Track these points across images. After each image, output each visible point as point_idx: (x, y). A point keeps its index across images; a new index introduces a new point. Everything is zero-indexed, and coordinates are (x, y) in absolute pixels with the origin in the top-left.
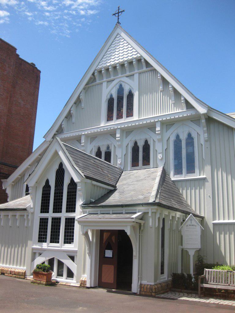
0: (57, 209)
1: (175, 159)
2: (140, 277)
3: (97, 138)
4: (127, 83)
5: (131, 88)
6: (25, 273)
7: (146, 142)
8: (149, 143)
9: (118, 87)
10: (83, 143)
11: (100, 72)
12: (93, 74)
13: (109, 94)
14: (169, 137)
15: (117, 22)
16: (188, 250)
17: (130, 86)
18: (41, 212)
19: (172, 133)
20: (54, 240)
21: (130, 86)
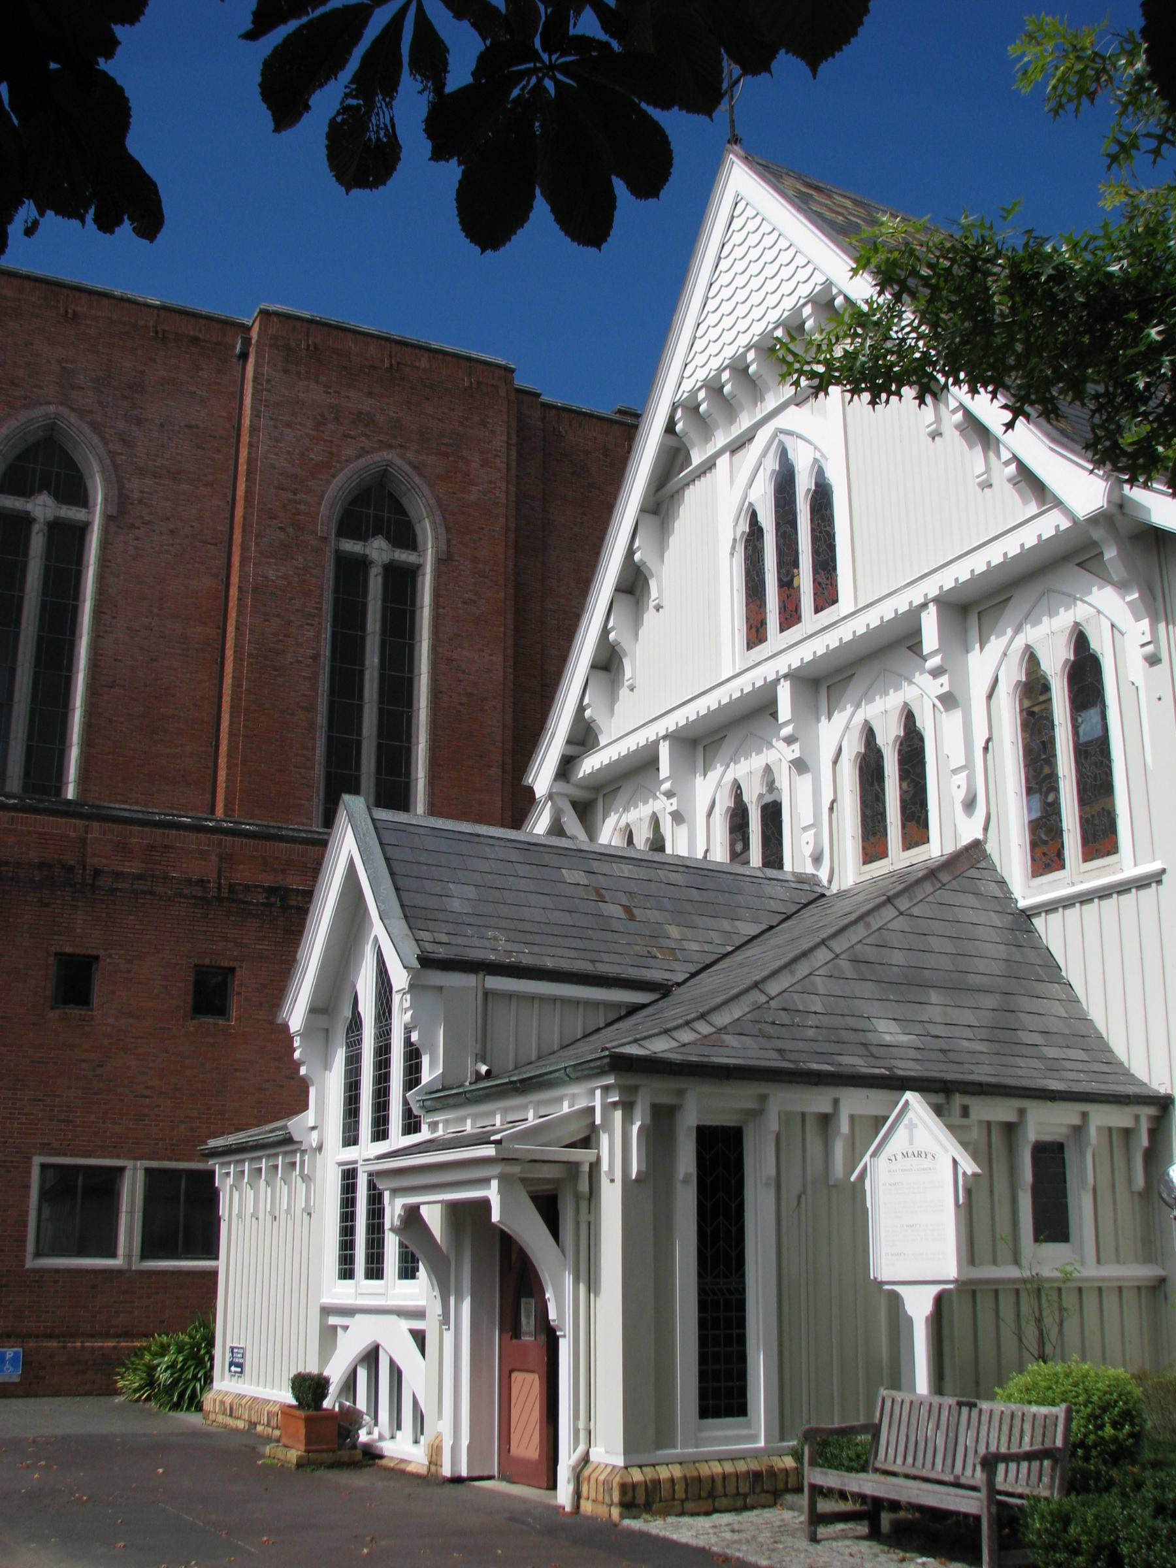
0: (37, 1129)
1: (1029, 791)
2: (581, 1424)
3: (855, 678)
4: (799, 436)
5: (818, 455)
6: (199, 1408)
7: (1080, 641)
8: (1094, 645)
9: (771, 464)
10: (933, 654)
11: (692, 408)
12: (670, 428)
13: (743, 513)
14: (997, 676)
15: (729, 136)
16: (899, 1289)
17: (816, 448)
18: (404, 1134)
19: (1005, 654)
20: (375, 1271)
21: (816, 448)
